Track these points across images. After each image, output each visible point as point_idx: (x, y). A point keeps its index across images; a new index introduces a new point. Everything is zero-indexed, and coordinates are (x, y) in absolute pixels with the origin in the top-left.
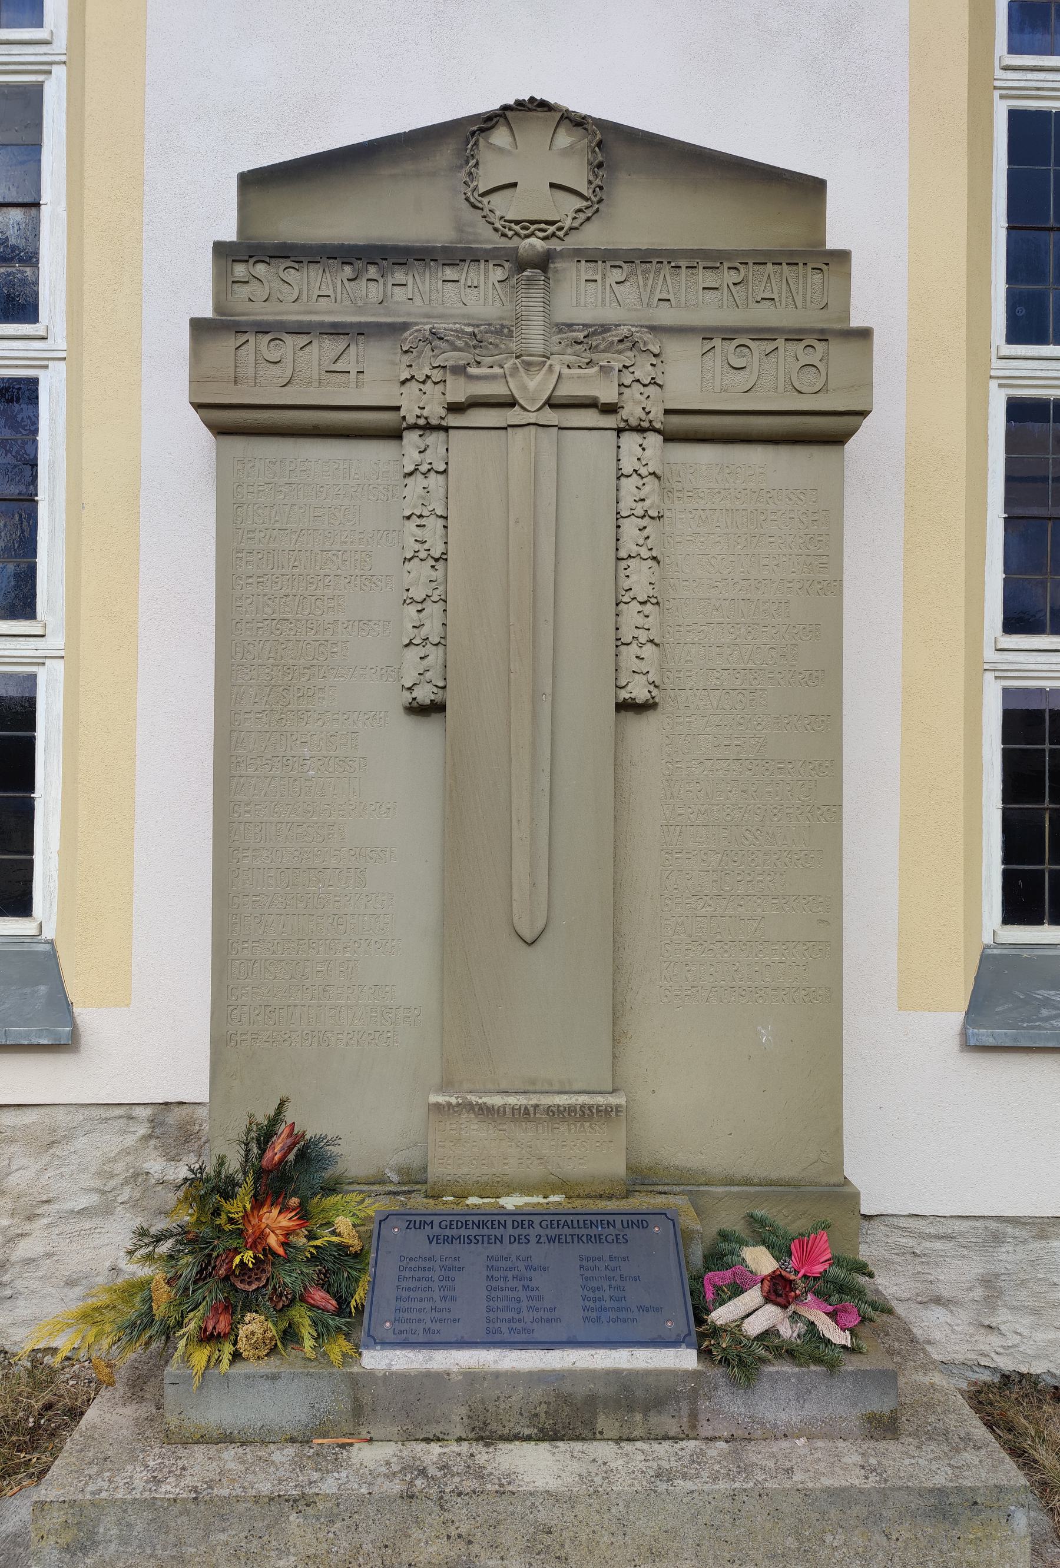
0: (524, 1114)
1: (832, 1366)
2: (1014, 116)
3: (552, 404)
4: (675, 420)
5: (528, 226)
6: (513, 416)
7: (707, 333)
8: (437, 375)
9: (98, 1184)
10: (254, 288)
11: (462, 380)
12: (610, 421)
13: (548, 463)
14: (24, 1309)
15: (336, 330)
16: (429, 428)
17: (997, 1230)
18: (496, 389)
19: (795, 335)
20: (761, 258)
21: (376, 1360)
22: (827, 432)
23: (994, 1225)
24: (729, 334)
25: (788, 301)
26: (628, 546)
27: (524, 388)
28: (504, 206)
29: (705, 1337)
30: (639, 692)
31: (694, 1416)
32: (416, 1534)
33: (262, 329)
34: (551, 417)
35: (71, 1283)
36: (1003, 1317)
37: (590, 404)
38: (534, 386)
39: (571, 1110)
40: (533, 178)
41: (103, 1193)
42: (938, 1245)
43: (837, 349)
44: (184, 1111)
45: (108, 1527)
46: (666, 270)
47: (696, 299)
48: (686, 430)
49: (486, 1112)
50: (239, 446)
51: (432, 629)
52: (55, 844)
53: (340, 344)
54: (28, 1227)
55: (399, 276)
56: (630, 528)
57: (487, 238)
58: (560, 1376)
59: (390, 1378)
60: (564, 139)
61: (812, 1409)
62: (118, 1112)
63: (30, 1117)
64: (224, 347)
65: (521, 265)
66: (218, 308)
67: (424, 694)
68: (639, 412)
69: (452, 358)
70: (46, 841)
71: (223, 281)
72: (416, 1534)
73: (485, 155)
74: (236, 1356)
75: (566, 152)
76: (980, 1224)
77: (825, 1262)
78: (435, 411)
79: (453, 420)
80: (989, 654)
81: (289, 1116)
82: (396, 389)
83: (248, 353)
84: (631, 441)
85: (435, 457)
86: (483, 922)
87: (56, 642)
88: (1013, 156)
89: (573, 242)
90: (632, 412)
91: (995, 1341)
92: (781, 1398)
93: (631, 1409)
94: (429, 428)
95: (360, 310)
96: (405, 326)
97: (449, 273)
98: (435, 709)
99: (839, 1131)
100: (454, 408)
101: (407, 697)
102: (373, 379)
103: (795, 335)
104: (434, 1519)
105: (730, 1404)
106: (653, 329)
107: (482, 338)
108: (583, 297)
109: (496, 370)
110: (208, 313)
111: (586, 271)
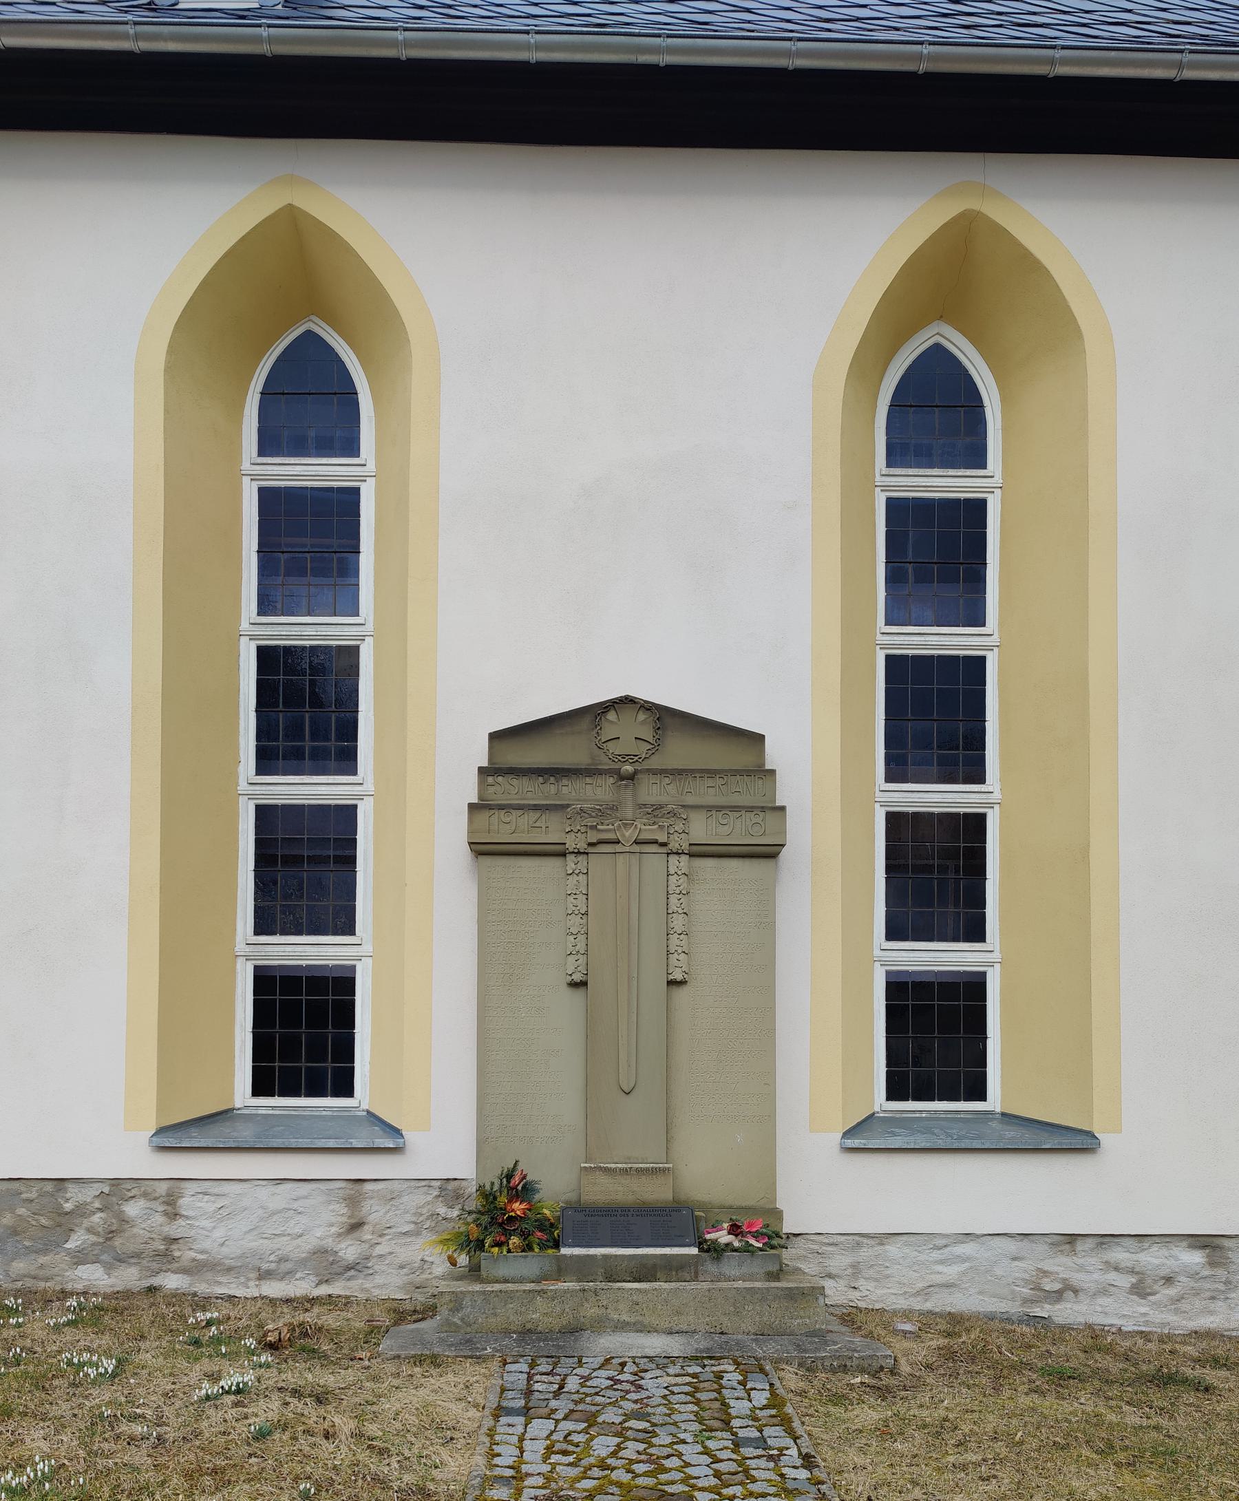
0: (625, 1172)
1: (753, 1252)
2: (889, 658)
3: (636, 842)
4: (695, 848)
5: (625, 758)
6: (618, 848)
7: (709, 808)
8: (583, 829)
9: (414, 1219)
10: (497, 788)
11: (595, 832)
12: (664, 850)
13: (635, 870)
14: (379, 1280)
15: (536, 808)
16: (579, 853)
17: (860, 1239)
18: (611, 836)
19: (750, 809)
20: (735, 773)
21: (565, 1251)
22: (769, 853)
23: (857, 1238)
24: (719, 808)
25: (744, 792)
26: (673, 908)
27: (623, 835)
28: (613, 748)
29: (701, 1243)
30: (678, 976)
31: (696, 1273)
32: (586, 1305)
33: (501, 807)
34: (637, 848)
35: (402, 1267)
36: (861, 1283)
37: (655, 842)
38: (629, 834)
39: (647, 1169)
40: (627, 734)
41: (416, 1223)
42: (830, 1248)
43: (769, 816)
44: (456, 1183)
45: (467, 1301)
46: (690, 779)
47: (707, 792)
48: (698, 852)
49: (607, 1170)
50: (487, 861)
51: (581, 947)
52: (367, 1058)
53: (538, 814)
54: (380, 1240)
55: (565, 782)
56: (673, 900)
57: (606, 764)
58: (642, 1256)
59: (572, 1256)
60: (642, 716)
61: (745, 1269)
62: (424, 1183)
63: (380, 1186)
64: (483, 817)
65: (622, 778)
66: (480, 798)
67: (577, 977)
68: (677, 846)
69: (591, 822)
70: (362, 1056)
71: (482, 784)
72: (586, 1305)
73: (604, 724)
74: (509, 1251)
75: (643, 723)
76: (850, 1238)
77: (762, 1234)
78: (582, 846)
79: (590, 850)
80: (877, 952)
81: (519, 1168)
82: (564, 835)
83: (495, 819)
84: (673, 859)
85: (582, 866)
86: (608, 1075)
87: (367, 948)
88: (888, 680)
89: (646, 765)
90: (674, 846)
91: (857, 1294)
92: (731, 1266)
93: (671, 1270)
94: (579, 853)
95: (546, 798)
96: (568, 806)
97: (588, 780)
98: (583, 984)
99: (774, 1183)
100: (590, 844)
101: (569, 979)
102: (552, 831)
103: (750, 809)
104: (593, 1299)
105: (711, 1267)
106: (683, 806)
107: (606, 811)
108: (652, 791)
109: (611, 827)
110: (475, 801)
111: (653, 779)
